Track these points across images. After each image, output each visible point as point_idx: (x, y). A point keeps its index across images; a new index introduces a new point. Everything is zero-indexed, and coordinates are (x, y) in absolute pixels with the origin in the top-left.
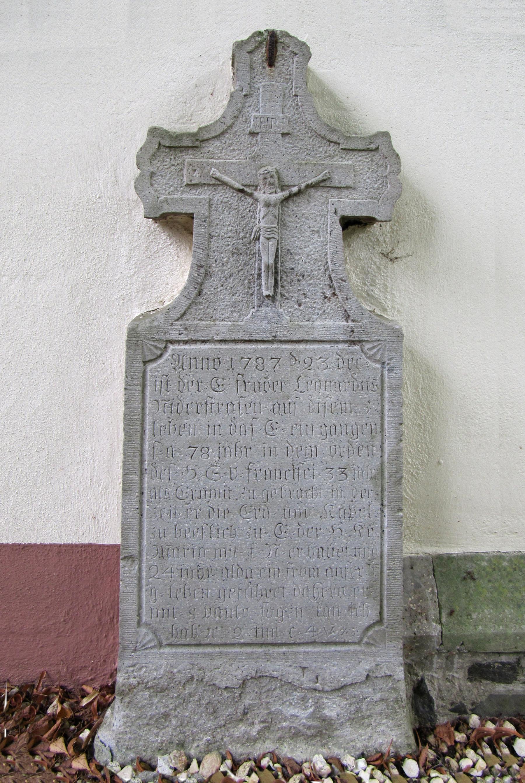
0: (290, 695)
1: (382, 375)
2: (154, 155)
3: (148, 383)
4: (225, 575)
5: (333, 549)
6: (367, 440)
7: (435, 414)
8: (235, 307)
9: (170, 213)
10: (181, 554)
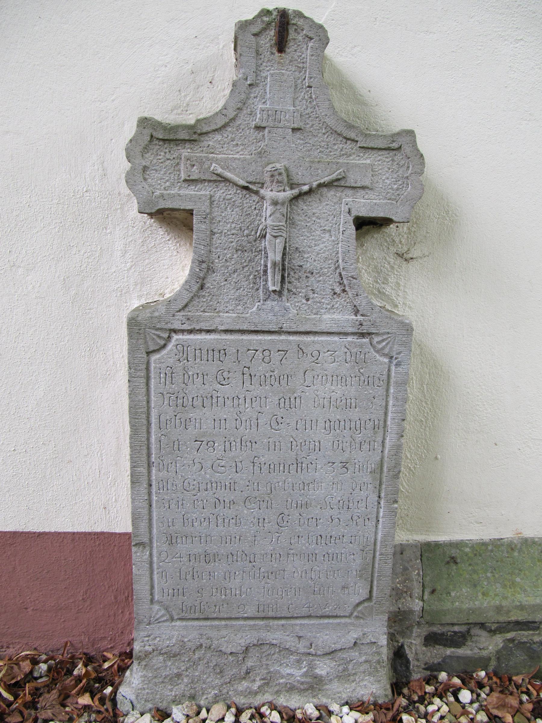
0: (287, 658)
1: (389, 370)
2: (146, 148)
3: (152, 375)
4: (230, 559)
5: (331, 537)
6: (369, 435)
7: (437, 410)
8: (240, 301)
9: (167, 209)
10: (189, 541)
